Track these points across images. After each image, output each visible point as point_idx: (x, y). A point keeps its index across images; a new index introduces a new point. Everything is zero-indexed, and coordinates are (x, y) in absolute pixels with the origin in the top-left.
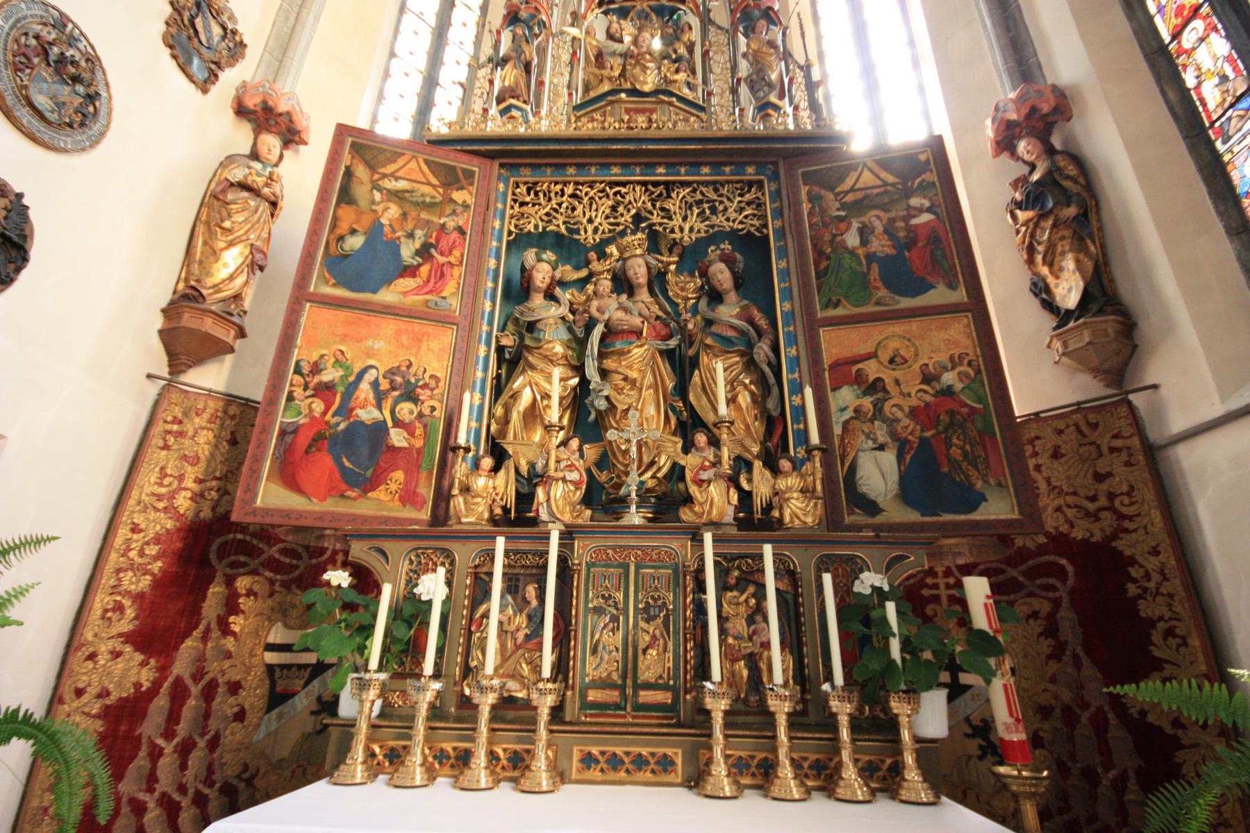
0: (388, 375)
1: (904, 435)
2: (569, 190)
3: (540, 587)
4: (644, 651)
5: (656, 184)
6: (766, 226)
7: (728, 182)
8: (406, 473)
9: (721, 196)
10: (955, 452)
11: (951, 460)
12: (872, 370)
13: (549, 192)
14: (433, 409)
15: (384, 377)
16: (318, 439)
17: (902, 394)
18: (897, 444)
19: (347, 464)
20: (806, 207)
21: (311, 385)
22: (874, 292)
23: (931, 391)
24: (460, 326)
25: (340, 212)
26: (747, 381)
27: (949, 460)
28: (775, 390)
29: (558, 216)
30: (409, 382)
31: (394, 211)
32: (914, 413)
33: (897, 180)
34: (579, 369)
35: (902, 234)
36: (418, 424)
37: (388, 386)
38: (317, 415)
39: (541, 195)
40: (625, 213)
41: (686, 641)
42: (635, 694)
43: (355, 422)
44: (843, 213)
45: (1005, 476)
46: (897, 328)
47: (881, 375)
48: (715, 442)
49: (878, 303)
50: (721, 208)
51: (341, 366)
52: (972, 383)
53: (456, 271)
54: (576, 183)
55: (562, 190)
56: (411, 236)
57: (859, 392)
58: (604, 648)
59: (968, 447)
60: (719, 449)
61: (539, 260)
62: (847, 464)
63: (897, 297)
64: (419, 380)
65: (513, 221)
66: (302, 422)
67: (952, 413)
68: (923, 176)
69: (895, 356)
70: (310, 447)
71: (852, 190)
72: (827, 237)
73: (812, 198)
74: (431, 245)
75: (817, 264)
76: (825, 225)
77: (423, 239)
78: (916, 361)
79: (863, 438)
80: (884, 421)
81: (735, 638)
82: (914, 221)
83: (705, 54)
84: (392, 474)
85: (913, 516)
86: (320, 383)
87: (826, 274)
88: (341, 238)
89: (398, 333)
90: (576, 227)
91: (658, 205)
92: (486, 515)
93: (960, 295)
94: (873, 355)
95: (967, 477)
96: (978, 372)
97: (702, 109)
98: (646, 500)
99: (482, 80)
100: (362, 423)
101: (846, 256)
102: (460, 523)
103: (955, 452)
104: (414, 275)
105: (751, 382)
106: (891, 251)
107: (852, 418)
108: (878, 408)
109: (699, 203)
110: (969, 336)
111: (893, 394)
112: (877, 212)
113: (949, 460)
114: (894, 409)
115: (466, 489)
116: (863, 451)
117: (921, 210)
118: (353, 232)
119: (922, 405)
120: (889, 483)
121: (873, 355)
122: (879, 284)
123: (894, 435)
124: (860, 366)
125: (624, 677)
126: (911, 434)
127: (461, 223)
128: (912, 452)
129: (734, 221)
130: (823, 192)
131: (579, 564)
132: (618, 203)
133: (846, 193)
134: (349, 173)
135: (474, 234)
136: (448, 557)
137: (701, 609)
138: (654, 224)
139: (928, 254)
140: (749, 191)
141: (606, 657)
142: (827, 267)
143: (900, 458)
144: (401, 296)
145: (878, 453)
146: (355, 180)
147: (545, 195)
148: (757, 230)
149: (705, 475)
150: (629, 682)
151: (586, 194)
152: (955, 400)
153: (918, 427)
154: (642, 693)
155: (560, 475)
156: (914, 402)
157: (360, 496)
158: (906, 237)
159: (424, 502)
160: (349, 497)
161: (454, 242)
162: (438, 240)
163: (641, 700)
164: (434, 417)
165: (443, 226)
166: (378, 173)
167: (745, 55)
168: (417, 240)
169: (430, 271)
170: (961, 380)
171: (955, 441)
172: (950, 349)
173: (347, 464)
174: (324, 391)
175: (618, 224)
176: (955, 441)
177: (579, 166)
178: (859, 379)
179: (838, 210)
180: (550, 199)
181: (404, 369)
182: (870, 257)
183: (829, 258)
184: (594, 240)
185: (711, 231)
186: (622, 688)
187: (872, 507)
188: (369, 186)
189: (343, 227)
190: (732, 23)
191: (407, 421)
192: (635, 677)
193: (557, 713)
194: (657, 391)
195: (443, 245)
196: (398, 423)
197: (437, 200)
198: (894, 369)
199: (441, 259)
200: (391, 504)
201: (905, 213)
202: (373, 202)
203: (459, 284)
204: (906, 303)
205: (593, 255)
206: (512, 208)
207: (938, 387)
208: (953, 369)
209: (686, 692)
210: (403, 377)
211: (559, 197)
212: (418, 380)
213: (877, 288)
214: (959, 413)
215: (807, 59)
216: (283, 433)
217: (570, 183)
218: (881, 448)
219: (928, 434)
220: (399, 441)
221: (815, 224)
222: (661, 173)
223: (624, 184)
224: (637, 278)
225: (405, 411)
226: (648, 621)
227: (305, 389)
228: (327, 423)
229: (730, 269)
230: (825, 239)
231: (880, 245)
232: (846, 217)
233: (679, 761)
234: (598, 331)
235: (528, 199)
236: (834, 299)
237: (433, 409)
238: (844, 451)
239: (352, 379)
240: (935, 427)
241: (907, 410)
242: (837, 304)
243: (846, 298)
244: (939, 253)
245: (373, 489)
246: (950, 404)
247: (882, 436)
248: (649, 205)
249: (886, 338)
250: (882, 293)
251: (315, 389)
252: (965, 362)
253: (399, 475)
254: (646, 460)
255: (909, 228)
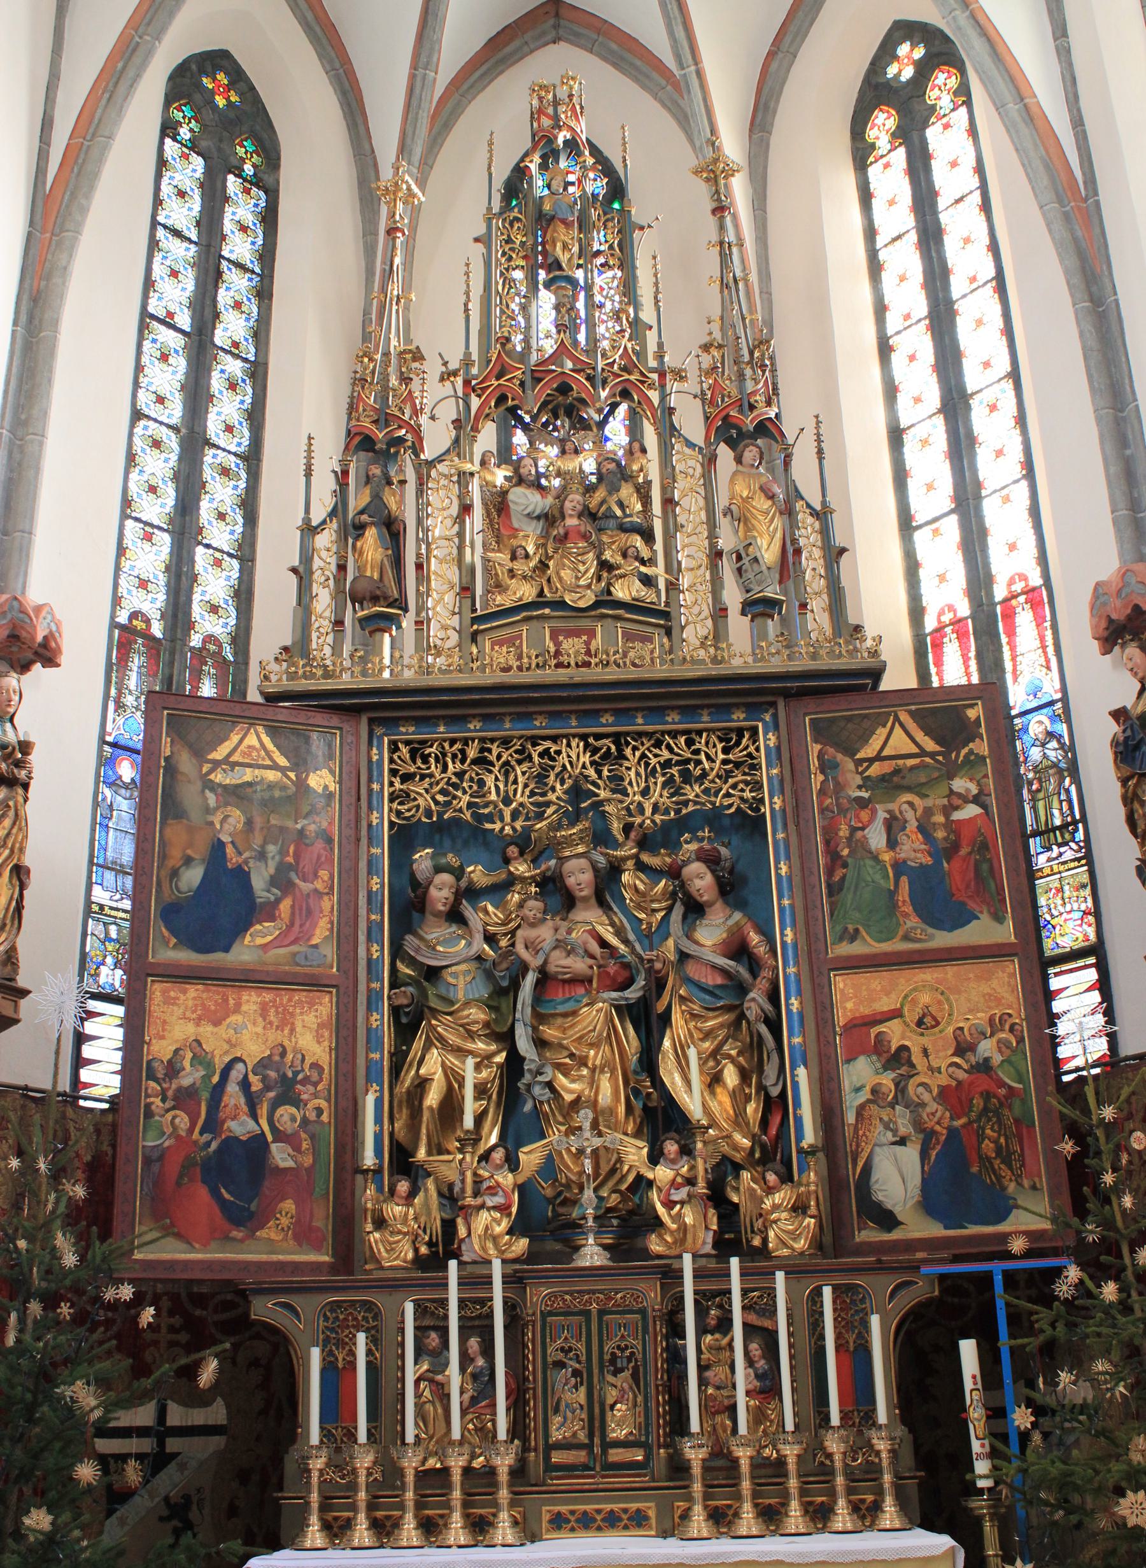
0: (259, 1070)
1: (929, 1125)
2: (472, 753)
3: (483, 1340)
4: (612, 1407)
5: (598, 737)
6: (762, 801)
7: (708, 730)
8: (296, 1203)
9: (697, 752)
10: (988, 1147)
11: (985, 1160)
12: (895, 1033)
13: (444, 755)
14: (319, 1111)
15: (255, 1074)
16: (188, 1165)
17: (931, 1069)
18: (921, 1136)
19: (227, 1196)
20: (817, 780)
21: (170, 1093)
22: (901, 920)
23: (966, 1067)
24: (342, 990)
25: (168, 831)
26: (733, 1052)
27: (980, 1157)
28: (775, 1057)
29: (459, 793)
30: (285, 1075)
31: (236, 817)
32: (944, 1095)
33: (938, 748)
34: (507, 1039)
35: (940, 834)
36: (303, 1135)
37: (261, 1086)
38: (183, 1134)
39: (432, 760)
40: (558, 786)
41: (658, 1393)
42: (604, 1452)
43: (228, 1138)
44: (866, 795)
45: (1040, 1177)
46: (927, 975)
47: (907, 1043)
48: (686, 1151)
49: (906, 938)
50: (698, 772)
51: (201, 1063)
52: (1011, 1052)
53: (326, 904)
54: (483, 740)
55: (463, 752)
56: (262, 856)
57: (879, 1065)
58: (567, 1406)
59: (1002, 1140)
60: (694, 1159)
61: (438, 870)
62: (860, 1164)
63: (930, 930)
64: (298, 1072)
65: (395, 805)
66: (167, 1144)
67: (987, 1096)
68: (971, 745)
69: (924, 1016)
70: (181, 1176)
71: (878, 758)
72: (844, 831)
73: (826, 766)
74: (290, 867)
75: (830, 872)
76: (843, 811)
77: (277, 858)
78: (949, 1024)
79: (881, 1128)
80: (907, 1107)
81: (718, 1388)
82: (957, 816)
83: (669, 502)
84: (281, 1205)
85: (935, 1230)
86: (180, 1089)
87: (841, 889)
88: (175, 873)
89: (264, 1010)
90: (486, 811)
91: (605, 773)
92: (410, 1255)
93: (1006, 932)
94: (896, 1014)
95: (999, 1178)
96: (1021, 1040)
97: (666, 615)
98: (606, 1222)
99: (324, 554)
100: (236, 1138)
101: (869, 862)
102: (382, 1268)
103: (988, 1147)
104: (272, 918)
105: (739, 1053)
106: (927, 860)
107: (869, 1101)
108: (900, 1086)
109: (667, 764)
110: (1014, 989)
111: (919, 1067)
112: (908, 797)
113: (980, 1157)
114: (921, 1089)
115: (380, 1223)
116: (880, 1146)
117: (966, 799)
118: (188, 861)
119: (954, 1083)
120: (910, 1186)
121: (896, 1014)
122: (909, 909)
123: (918, 1125)
124: (882, 1028)
125: (591, 1435)
126: (938, 1123)
127: (325, 824)
128: (939, 1147)
129: (716, 794)
130: (840, 757)
131: (534, 1314)
132: (545, 770)
133: (871, 761)
134: (171, 770)
135: (821, 936)
136: (369, 1310)
137: (677, 1358)
138: (601, 803)
139: (972, 867)
140: (738, 743)
141: (569, 1414)
142: (843, 878)
143: (924, 1155)
144: (261, 952)
145: (898, 1149)
146: (179, 777)
147: (437, 760)
148: (750, 808)
149: (677, 1196)
150: (597, 1440)
151: (499, 757)
152: (990, 1077)
153: (948, 1114)
154: (611, 1451)
155: (479, 1201)
156: (944, 1080)
157: (247, 1237)
158: (946, 839)
159: (324, 1239)
160: (234, 1239)
161: (319, 857)
162: (297, 856)
163: (611, 1459)
164: (322, 1123)
165: (301, 832)
166: (209, 761)
167: (728, 512)
168: (270, 862)
169: (293, 907)
170: (1000, 1051)
171: (988, 1132)
172: (990, 1008)
173: (227, 1196)
174: (184, 1099)
175: (548, 804)
176: (988, 1132)
177: (485, 718)
178: (879, 1047)
179: (860, 787)
180: (445, 769)
181: (277, 1058)
182: (900, 867)
183: (845, 865)
184: (514, 829)
185: (684, 811)
186: (589, 1447)
187: (888, 1220)
188: (199, 784)
189: (176, 854)
190: (707, 437)
191: (289, 1131)
192: (603, 1435)
193: (518, 1473)
194: (613, 1071)
195: (306, 864)
196: (279, 1136)
197: (290, 792)
198: (922, 1034)
199: (305, 887)
200: (285, 1244)
201: (945, 801)
202: (208, 810)
203: (332, 923)
204: (943, 939)
205: (513, 851)
206: (391, 784)
207: (973, 1060)
208: (992, 1035)
209: (659, 1447)
210: (278, 1071)
211: (458, 765)
212: (296, 1073)
213: (906, 915)
214: (995, 1096)
215: (824, 503)
216: (147, 1161)
217: (473, 740)
218: (902, 1142)
219: (958, 1123)
220: (283, 1160)
221: (827, 809)
222: (607, 723)
223: (555, 739)
224: (701, 896)
225: (286, 1118)
226: (615, 1374)
227: (164, 1100)
228: (196, 1142)
229: (713, 872)
230: (841, 834)
231: (913, 849)
232: (869, 800)
233: (652, 1513)
234: (530, 979)
235: (412, 769)
236: (851, 928)
237: (319, 1111)
238: (858, 1145)
239: (216, 1079)
240: (966, 1114)
241: (935, 1091)
242: (854, 937)
243: (867, 927)
244: (985, 867)
245: (261, 1227)
246: (984, 1083)
247: (904, 1126)
248: (591, 772)
249: (915, 990)
250: (913, 922)
251: (175, 1098)
252: (1007, 1027)
253: (289, 1205)
254: (604, 1169)
255: (949, 824)
